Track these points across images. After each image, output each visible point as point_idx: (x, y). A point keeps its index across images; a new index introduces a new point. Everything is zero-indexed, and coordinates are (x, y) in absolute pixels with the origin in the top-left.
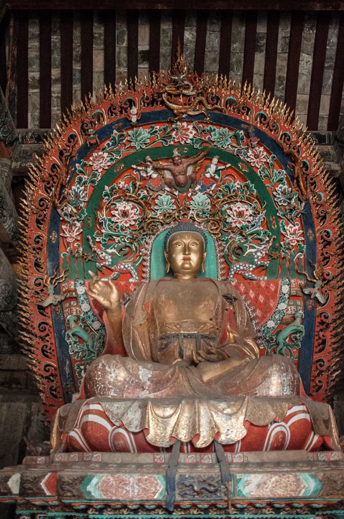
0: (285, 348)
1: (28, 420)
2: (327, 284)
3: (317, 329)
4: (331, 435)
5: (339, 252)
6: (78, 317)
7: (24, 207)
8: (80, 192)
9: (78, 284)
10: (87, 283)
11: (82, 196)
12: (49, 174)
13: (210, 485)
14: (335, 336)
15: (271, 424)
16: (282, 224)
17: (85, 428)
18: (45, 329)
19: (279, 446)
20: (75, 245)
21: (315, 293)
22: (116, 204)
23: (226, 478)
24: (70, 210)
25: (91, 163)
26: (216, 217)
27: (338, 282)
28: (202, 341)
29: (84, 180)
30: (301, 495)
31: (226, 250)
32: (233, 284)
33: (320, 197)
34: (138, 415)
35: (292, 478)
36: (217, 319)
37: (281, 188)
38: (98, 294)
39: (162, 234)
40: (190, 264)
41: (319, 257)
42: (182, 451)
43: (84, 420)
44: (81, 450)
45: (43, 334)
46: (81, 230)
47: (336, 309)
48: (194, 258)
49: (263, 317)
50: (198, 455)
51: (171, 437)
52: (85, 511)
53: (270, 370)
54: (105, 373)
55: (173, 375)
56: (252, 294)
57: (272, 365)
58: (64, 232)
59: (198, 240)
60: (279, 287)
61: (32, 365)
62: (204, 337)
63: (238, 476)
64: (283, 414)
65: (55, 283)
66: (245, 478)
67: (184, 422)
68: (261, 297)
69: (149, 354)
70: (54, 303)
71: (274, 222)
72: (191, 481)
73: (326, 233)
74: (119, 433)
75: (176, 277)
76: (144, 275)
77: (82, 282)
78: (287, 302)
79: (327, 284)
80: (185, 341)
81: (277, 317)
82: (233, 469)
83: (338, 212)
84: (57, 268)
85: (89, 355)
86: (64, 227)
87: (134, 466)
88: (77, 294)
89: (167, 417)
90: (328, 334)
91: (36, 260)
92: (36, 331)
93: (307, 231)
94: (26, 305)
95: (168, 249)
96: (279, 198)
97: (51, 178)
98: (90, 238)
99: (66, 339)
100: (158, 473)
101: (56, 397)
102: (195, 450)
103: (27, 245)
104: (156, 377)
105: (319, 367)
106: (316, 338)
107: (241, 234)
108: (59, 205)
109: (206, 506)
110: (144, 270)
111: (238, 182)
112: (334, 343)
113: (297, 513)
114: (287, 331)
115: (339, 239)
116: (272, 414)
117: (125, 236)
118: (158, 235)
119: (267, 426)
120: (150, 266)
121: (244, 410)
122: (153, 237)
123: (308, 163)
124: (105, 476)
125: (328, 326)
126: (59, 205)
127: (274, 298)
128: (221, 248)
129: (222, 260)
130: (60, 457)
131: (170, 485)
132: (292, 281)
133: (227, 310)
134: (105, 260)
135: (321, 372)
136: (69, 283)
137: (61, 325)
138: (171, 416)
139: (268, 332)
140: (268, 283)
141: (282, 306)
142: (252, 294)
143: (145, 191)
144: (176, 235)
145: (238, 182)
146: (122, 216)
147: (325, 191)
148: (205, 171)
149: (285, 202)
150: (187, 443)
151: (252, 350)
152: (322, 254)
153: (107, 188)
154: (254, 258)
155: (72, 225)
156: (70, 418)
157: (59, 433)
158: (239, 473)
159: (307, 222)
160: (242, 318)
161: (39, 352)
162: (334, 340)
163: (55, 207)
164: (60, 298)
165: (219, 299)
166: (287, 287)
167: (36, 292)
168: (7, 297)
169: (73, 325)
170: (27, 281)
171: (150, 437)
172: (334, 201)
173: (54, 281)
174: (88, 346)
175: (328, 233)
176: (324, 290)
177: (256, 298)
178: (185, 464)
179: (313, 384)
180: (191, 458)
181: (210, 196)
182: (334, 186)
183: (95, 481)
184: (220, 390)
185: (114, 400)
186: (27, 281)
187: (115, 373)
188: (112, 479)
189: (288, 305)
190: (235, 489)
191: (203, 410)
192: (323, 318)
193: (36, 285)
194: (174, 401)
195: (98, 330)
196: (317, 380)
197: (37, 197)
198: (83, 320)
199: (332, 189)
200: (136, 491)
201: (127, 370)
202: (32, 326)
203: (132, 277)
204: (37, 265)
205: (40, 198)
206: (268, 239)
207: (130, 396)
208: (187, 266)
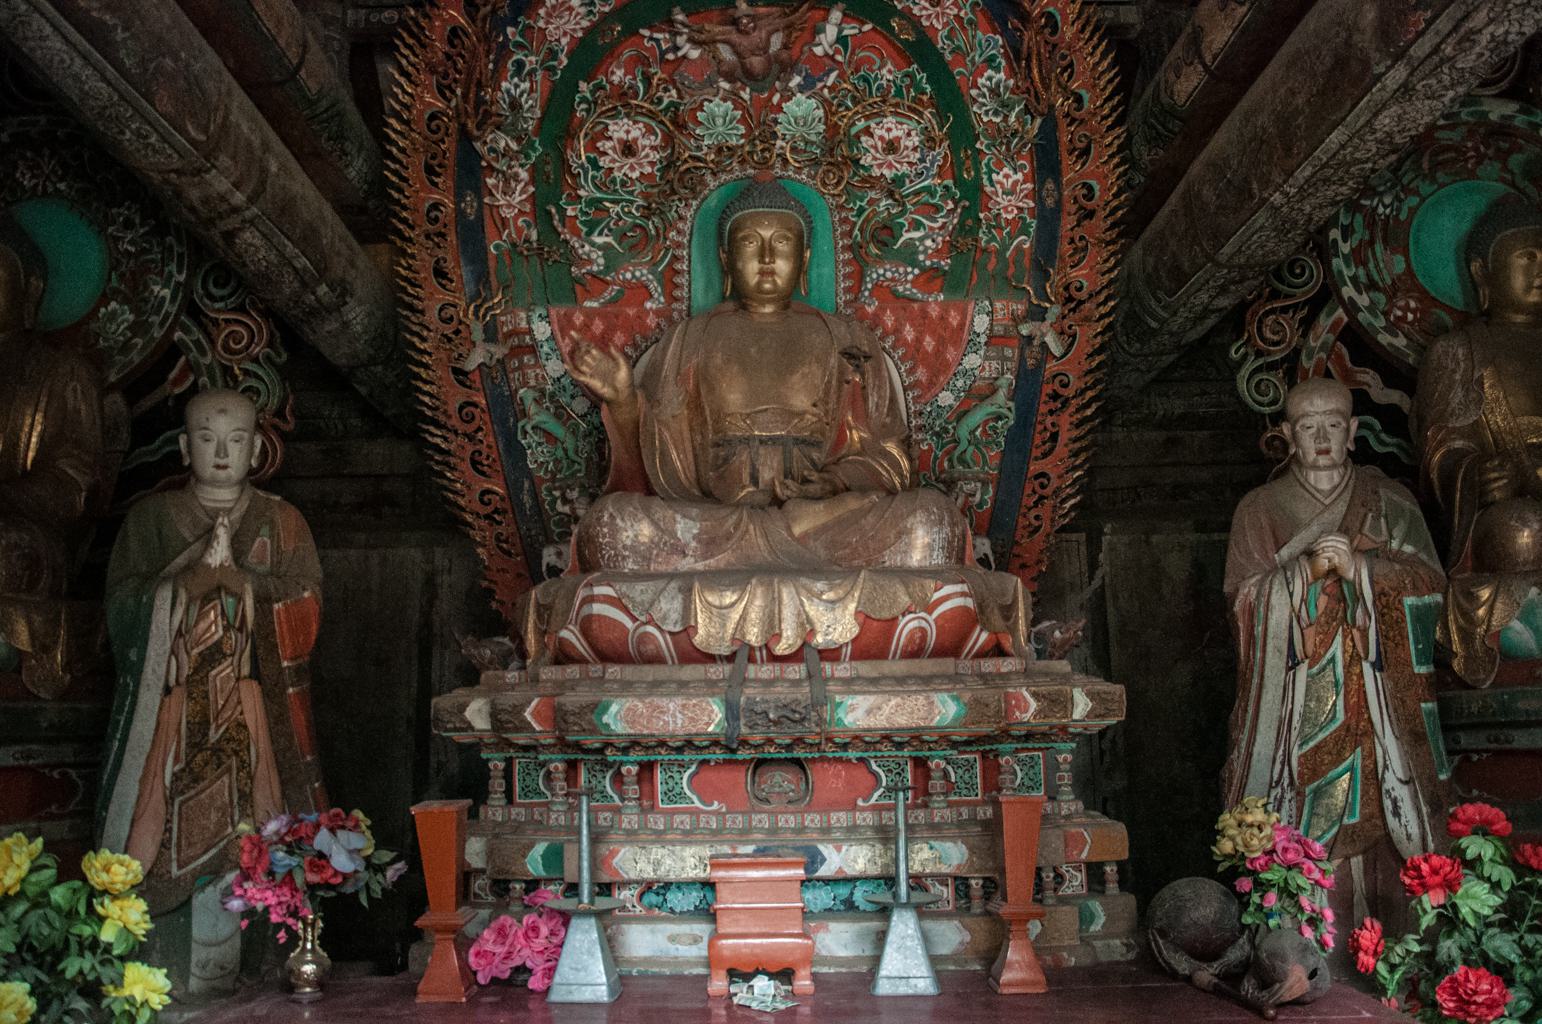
0: (971, 449)
1: (430, 582)
2: (1073, 310)
3: (1044, 409)
4: (1013, 630)
5: (1114, 233)
6: (542, 392)
7: (393, 136)
8: (521, 95)
9: (535, 318)
10: (553, 313)
11: (526, 106)
12: (446, 53)
13: (794, 712)
14: (1077, 426)
15: (904, 615)
16: (987, 165)
17: (587, 626)
18: (473, 418)
19: (914, 652)
20: (520, 222)
21: (1043, 335)
22: (607, 125)
23: (818, 703)
24: (502, 144)
25: (541, 24)
26: (836, 153)
27: (1099, 305)
28: (795, 451)
29: (527, 68)
30: (933, 724)
31: (856, 232)
32: (870, 309)
33: (1079, 99)
34: (677, 604)
35: (921, 699)
36: (827, 403)
37: (990, 79)
38: (591, 376)
39: (715, 194)
40: (774, 283)
41: (1065, 248)
42: (751, 660)
43: (585, 610)
44: (580, 660)
45: (470, 428)
46: (532, 189)
47: (1086, 367)
48: (782, 266)
49: (931, 384)
50: (777, 667)
51: (733, 639)
52: (600, 751)
53: (911, 520)
54: (615, 531)
55: (737, 527)
56: (909, 334)
57: (913, 512)
58: (492, 195)
59: (789, 230)
60: (969, 318)
61: (455, 492)
62: (798, 441)
63: (838, 699)
64: (925, 598)
65: (484, 316)
66: (849, 700)
67: (754, 615)
68: (928, 339)
69: (692, 475)
70: (487, 361)
71: (969, 163)
72: (764, 706)
73: (1085, 191)
74: (646, 634)
75: (744, 307)
76: (677, 293)
77: (544, 313)
78: (982, 352)
79: (1073, 310)
80: (762, 451)
81: (960, 383)
82: (832, 687)
83: (1118, 137)
84: (482, 277)
85: (569, 468)
86: (490, 181)
87: (674, 686)
88: (533, 338)
89: (726, 607)
90: (1065, 421)
91: (437, 262)
92: (455, 422)
93: (1042, 183)
94: (426, 366)
95: (727, 247)
96: (984, 105)
97: (450, 63)
98: (553, 211)
99: (520, 437)
100: (713, 695)
101: (509, 554)
102: (775, 659)
103: (412, 228)
104: (706, 533)
105: (1037, 488)
106: (1040, 428)
107: (891, 195)
108: (476, 133)
109: (788, 741)
110: (678, 280)
111: (889, 66)
112: (1075, 440)
113: (930, 749)
114: (977, 417)
115: (1115, 203)
116: (904, 600)
117: (632, 202)
118: (706, 198)
119: (894, 620)
120: (689, 272)
121: (856, 595)
122: (694, 203)
123: (1059, 18)
124: (629, 702)
125: (1066, 402)
126: (476, 133)
127: (956, 343)
128: (847, 228)
129: (847, 256)
130: (548, 673)
131: (732, 712)
132: (998, 305)
133: (848, 382)
134: (590, 261)
135: (1042, 498)
136: (516, 316)
137: (506, 411)
138: (733, 605)
139: (939, 416)
140: (945, 308)
141: (972, 361)
142: (909, 334)
143: (674, 92)
144: (744, 217)
145: (889, 66)
146: (623, 153)
147: (1094, 86)
148: (812, 41)
149: (996, 113)
150: (760, 648)
151: (895, 464)
152: (1072, 241)
153: (583, 86)
154: (917, 253)
155: (509, 179)
156: (559, 605)
157: (541, 634)
158: (839, 693)
159: (1046, 163)
160: (880, 397)
161: (466, 466)
162: (1075, 433)
163: (465, 138)
164: (499, 351)
165: (833, 361)
166: (986, 319)
167: (445, 336)
168: (374, 339)
169: (532, 409)
170: (422, 312)
171: (698, 640)
172: (1114, 109)
173: (482, 311)
174: (565, 450)
175: (1090, 189)
176: (1067, 322)
177: (919, 340)
178: (757, 680)
179: (1022, 522)
180: (766, 671)
181: (825, 103)
182: (1116, 76)
183: (614, 708)
184: (822, 553)
185: (636, 577)
186: (422, 312)
187: (633, 529)
188: (640, 705)
189: (986, 358)
190: (832, 717)
191: (787, 594)
192: (1057, 386)
193: (443, 321)
194: (736, 577)
195: (585, 415)
196: (1033, 514)
197: (421, 112)
198: (552, 395)
199: (1110, 81)
200: (679, 722)
201: (655, 523)
202: (445, 412)
203: (651, 296)
204: (440, 273)
205: (429, 112)
206: (951, 205)
207: (662, 568)
208: (767, 286)
